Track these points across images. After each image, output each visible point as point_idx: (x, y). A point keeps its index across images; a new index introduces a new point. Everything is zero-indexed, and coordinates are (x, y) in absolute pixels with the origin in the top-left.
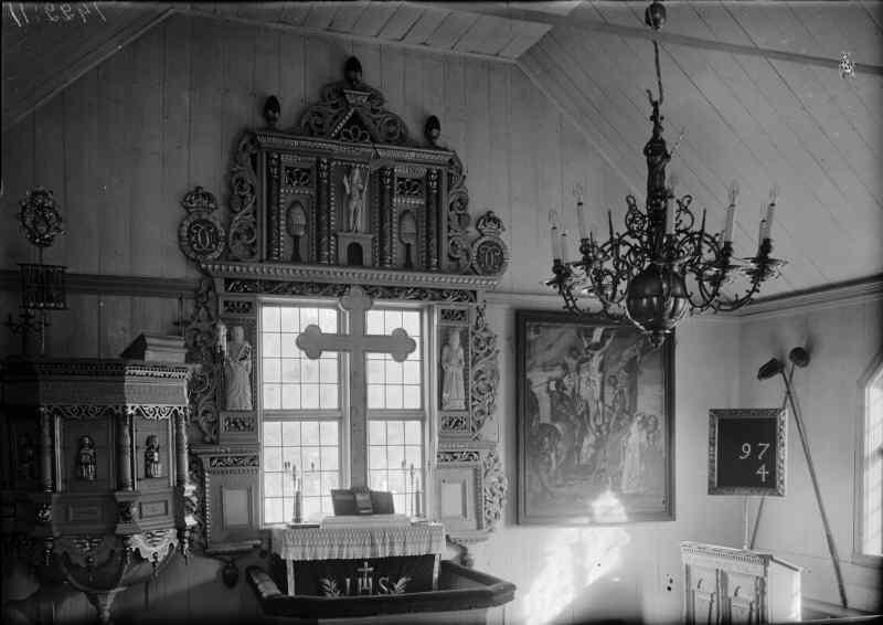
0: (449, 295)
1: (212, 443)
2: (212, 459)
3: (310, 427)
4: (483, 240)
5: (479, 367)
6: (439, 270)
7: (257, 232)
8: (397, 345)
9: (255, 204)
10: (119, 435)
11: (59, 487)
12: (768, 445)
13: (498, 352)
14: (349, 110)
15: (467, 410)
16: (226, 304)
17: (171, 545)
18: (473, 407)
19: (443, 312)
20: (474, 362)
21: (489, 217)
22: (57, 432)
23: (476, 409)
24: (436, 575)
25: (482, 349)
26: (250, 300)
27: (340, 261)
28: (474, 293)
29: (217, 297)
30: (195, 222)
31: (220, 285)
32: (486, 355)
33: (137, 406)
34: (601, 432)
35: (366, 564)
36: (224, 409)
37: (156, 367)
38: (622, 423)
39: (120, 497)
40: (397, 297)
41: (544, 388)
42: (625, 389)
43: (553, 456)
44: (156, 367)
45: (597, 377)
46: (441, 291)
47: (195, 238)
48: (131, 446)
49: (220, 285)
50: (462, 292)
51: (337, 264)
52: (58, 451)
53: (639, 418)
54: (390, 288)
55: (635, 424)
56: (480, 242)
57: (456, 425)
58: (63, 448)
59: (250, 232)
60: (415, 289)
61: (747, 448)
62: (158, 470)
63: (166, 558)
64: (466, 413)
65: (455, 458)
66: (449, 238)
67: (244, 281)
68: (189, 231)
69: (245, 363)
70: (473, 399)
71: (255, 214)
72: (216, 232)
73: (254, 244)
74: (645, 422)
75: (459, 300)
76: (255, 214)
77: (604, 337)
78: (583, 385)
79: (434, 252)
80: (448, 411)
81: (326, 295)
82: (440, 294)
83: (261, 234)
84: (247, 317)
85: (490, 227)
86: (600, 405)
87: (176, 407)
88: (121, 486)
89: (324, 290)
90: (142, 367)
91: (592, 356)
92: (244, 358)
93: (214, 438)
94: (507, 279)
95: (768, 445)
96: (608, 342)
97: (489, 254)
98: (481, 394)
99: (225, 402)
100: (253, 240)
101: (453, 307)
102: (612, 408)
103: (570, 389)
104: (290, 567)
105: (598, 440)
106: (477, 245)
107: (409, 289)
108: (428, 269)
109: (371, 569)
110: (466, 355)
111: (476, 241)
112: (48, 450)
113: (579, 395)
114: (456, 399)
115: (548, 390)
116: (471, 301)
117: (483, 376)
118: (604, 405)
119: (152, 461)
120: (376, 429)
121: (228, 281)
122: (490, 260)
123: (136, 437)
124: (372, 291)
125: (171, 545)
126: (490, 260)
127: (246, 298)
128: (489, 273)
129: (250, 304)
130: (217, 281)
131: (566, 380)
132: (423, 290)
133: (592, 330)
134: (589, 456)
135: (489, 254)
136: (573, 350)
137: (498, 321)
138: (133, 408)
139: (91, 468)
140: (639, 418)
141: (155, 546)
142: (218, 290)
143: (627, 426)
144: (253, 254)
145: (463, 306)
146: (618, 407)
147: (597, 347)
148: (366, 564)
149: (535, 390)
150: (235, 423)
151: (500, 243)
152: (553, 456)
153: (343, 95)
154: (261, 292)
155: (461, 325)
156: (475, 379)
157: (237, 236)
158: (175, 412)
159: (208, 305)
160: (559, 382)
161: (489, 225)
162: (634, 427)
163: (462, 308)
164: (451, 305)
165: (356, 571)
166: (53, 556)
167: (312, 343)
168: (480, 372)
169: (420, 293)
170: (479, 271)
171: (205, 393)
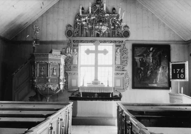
0: (117, 42)
1: (70, 70)
2: (70, 73)
3: (89, 68)
4: (125, 31)
5: (124, 56)
6: (115, 37)
7: (79, 31)
8: (105, 52)
9: (79, 27)
10: (48, 67)
11: (38, 76)
12: (179, 70)
13: (128, 53)
14: (97, 8)
15: (121, 64)
16: (73, 45)
17: (57, 88)
18: (122, 64)
19: (116, 45)
20: (123, 55)
21: (126, 26)
22: (38, 67)
23: (123, 64)
24: (160, 117)
25: (124, 52)
26: (78, 44)
27: (95, 36)
28: (123, 41)
29: (72, 44)
30: (68, 31)
31: (72, 42)
32: (125, 54)
33: (51, 62)
34: (152, 70)
35: (96, 94)
36: (72, 64)
37: (55, 55)
38: (157, 68)
39: (47, 78)
40: (106, 42)
41: (138, 60)
42: (158, 60)
43: (141, 74)
44: (55, 55)
45: (151, 58)
46: (115, 41)
47: (69, 33)
48: (50, 69)
49: (72, 42)
50: (120, 41)
51: (94, 37)
52: (38, 70)
53: (162, 67)
54: (105, 41)
55: (161, 68)
56: (124, 31)
57: (119, 67)
58: (39, 69)
59: (78, 32)
60: (110, 41)
61: (182, 71)
62: (55, 74)
63: (56, 90)
64: (121, 65)
65: (118, 74)
66: (117, 31)
67: (77, 41)
68: (67, 33)
69: (76, 56)
70: (122, 63)
71: (79, 29)
72: (72, 32)
73: (79, 34)
74: (163, 68)
75: (119, 43)
76: (79, 29)
77: (153, 50)
78: (148, 60)
79: (82, 33)
80: (117, 65)
81: (92, 43)
82: (115, 42)
83: (80, 32)
84: (77, 47)
85: (126, 28)
86: (152, 64)
87: (59, 62)
88: (47, 76)
89: (83, 42)
90: (52, 55)
91: (150, 53)
92: (76, 55)
93: (70, 69)
94: (130, 38)
95: (179, 70)
96: (154, 51)
97: (126, 33)
98: (124, 61)
99: (72, 63)
100: (78, 33)
101: (117, 44)
102: (155, 65)
103: (145, 61)
104: (81, 93)
105: (151, 71)
106: (123, 32)
107: (109, 41)
108: (113, 37)
109: (97, 95)
110: (121, 54)
111: (123, 31)
112: (36, 69)
113: (147, 62)
114: (118, 62)
115: (140, 61)
116: (122, 43)
117: (125, 58)
118: (153, 64)
119: (54, 72)
120: (99, 68)
121: (74, 41)
122: (126, 35)
123: (50, 68)
124: (101, 42)
125: (57, 88)
126: (126, 35)
127: (76, 44)
128: (126, 37)
129: (78, 45)
130: (71, 41)
131: (144, 59)
132: (112, 41)
133: (150, 48)
134: (149, 75)
135: (126, 33)
136: (145, 52)
137: (129, 47)
138: (50, 62)
139: (43, 73)
140: (162, 67)
141: (54, 87)
142: (72, 43)
143: (159, 68)
144: (78, 36)
145: (120, 44)
146: (156, 64)
147: (151, 51)
148: (96, 94)
149: (136, 61)
150: (74, 67)
151: (128, 31)
152: (141, 74)
153: (96, 6)
154: (79, 43)
155: (120, 48)
156: (123, 58)
157: (75, 33)
158: (59, 63)
159: (70, 45)
160: (142, 59)
161: (126, 28)
162: (160, 69)
163: (120, 44)
164: (117, 44)
165: (94, 95)
166: (36, 88)
167: (88, 52)
168: (124, 57)
169: (111, 42)
170: (124, 37)
171: (69, 61)
